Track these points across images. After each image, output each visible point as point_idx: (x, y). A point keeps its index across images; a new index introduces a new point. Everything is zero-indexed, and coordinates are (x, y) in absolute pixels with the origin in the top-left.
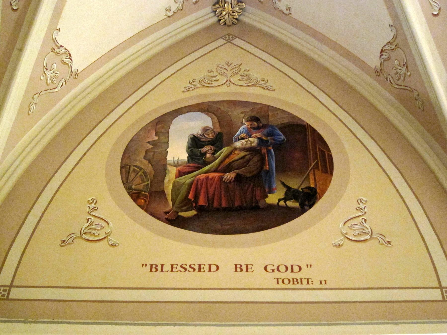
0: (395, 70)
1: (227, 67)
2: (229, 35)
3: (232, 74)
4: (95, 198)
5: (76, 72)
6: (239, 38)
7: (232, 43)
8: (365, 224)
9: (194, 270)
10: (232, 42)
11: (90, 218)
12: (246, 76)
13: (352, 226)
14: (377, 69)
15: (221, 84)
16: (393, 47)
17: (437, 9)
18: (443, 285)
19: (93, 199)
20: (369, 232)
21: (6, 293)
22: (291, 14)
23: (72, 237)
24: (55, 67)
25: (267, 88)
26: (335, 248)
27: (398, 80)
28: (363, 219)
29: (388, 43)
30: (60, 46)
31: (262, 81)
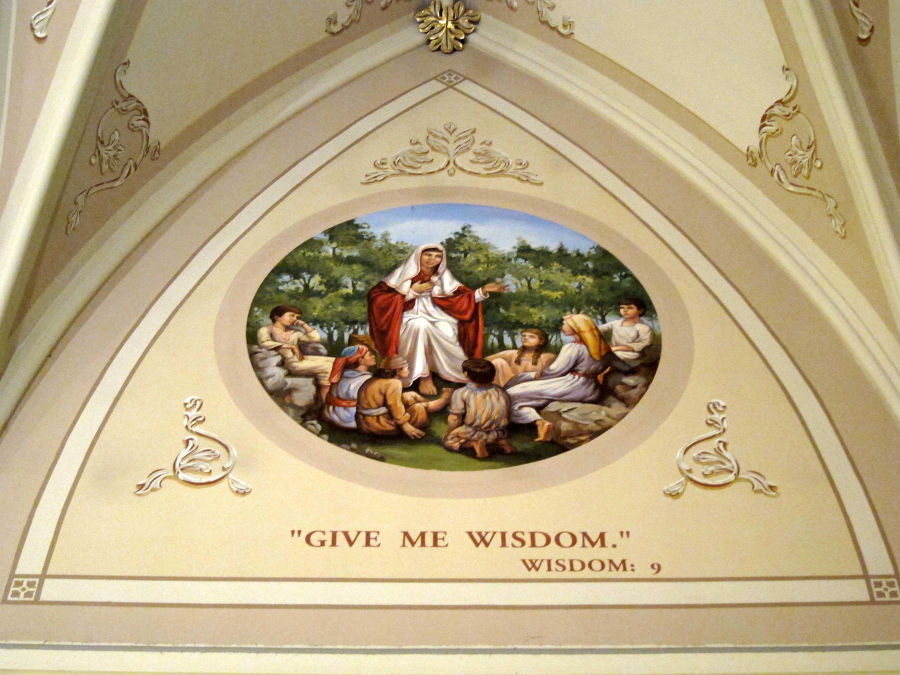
0: (790, 155)
1: (447, 135)
2: (450, 72)
3: (457, 150)
4: (197, 398)
5: (155, 146)
6: (470, 79)
7: (456, 89)
8: (725, 453)
9: (523, 543)
10: (456, 86)
11: (192, 439)
12: (486, 153)
13: (701, 457)
14: (752, 152)
15: (437, 169)
16: (789, 110)
17: (867, 29)
18: (871, 572)
19: (195, 400)
20: (733, 467)
21: (34, 590)
22: (572, 33)
23: (158, 477)
24: (117, 138)
25: (527, 180)
26: (670, 499)
27: (796, 176)
28: (720, 442)
29: (776, 103)
30: (128, 96)
31: (517, 164)
